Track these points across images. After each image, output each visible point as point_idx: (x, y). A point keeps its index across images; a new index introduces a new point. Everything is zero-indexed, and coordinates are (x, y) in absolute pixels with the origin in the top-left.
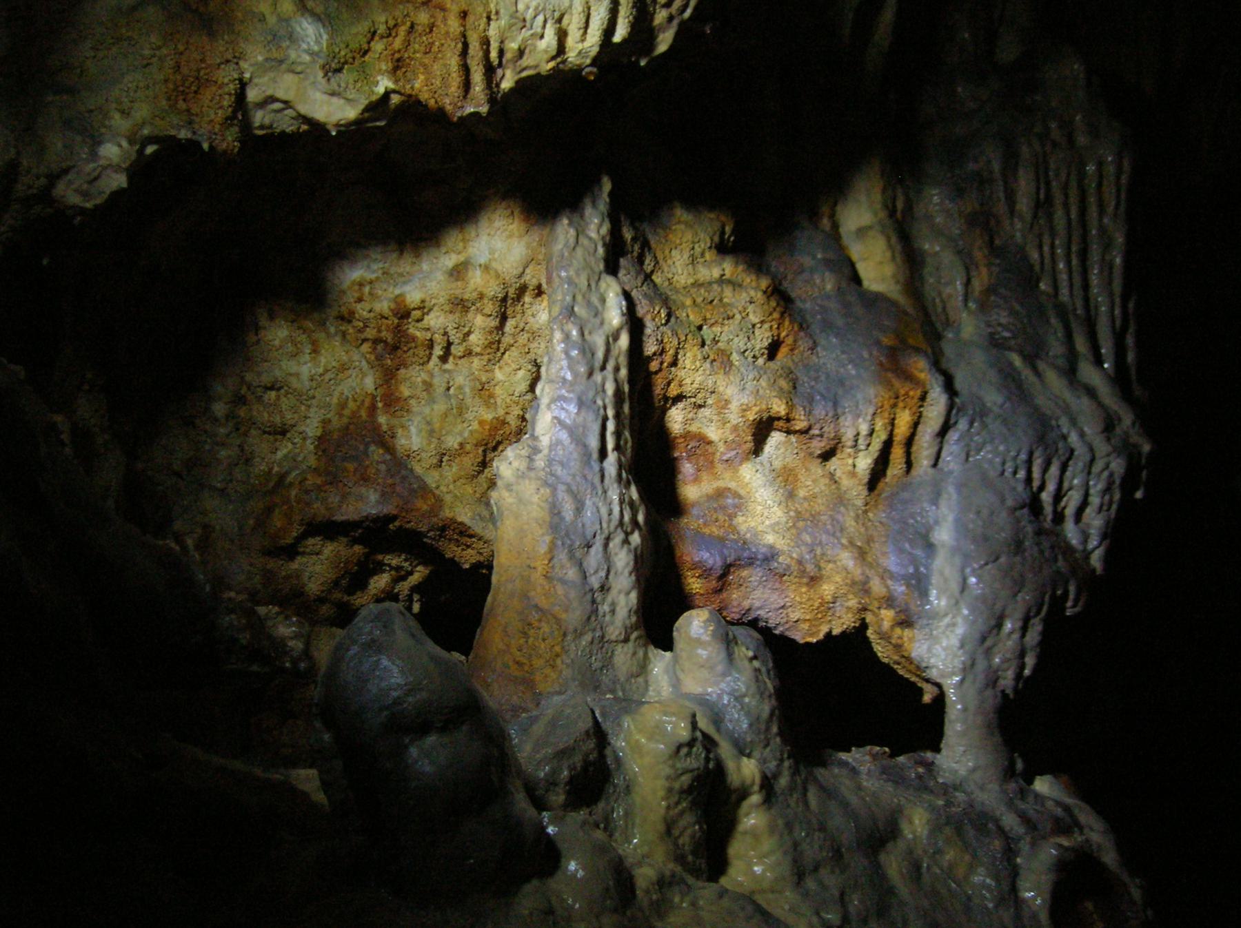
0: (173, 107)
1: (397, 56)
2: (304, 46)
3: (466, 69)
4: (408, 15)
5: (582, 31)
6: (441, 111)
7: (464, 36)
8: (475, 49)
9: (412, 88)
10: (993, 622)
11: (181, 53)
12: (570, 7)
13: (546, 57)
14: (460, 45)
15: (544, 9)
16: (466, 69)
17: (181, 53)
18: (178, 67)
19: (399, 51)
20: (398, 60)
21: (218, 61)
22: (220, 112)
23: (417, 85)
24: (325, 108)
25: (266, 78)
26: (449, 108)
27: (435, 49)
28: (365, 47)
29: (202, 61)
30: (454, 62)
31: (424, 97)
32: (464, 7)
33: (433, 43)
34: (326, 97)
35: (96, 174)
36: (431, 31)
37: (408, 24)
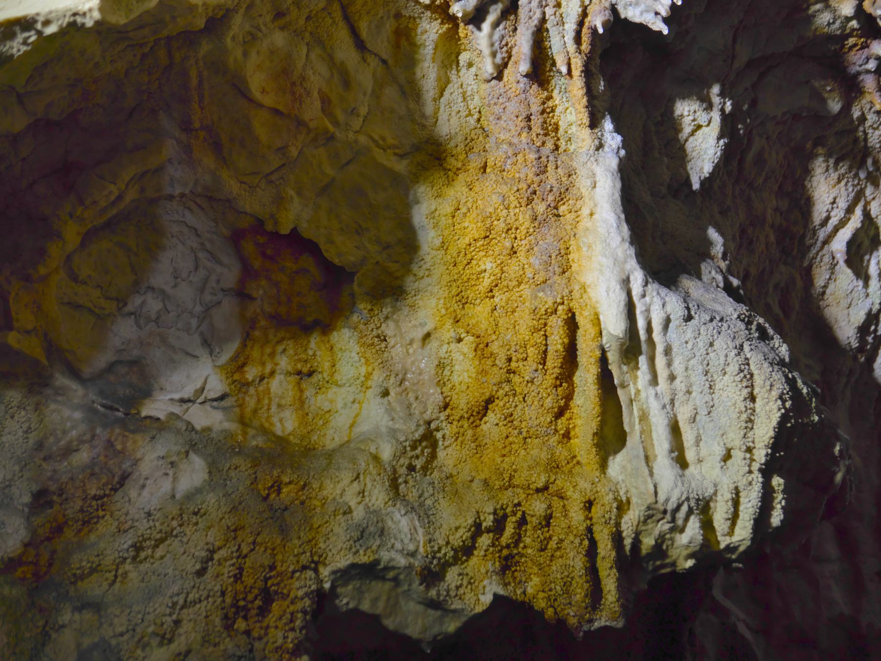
0: (228, 626)
1: (505, 552)
2: (398, 546)
3: (593, 571)
4: (519, 504)
5: (729, 522)
6: (561, 622)
7: (589, 530)
8: (605, 548)
9: (524, 593)
10: (245, 335)
11: (245, 556)
12: (715, 493)
13: (685, 553)
14: (586, 542)
15: (688, 499)
16: (593, 571)
17: (245, 556)
18: (238, 578)
19: (508, 546)
20: (506, 558)
21: (291, 568)
22: (291, 635)
23: (530, 591)
24: (420, 621)
25: (350, 587)
26: (573, 621)
27: (553, 544)
28: (469, 543)
29: (272, 567)
30: (579, 563)
31: (540, 604)
32: (590, 495)
33: (550, 538)
34: (420, 608)
35: (557, 340)
36: (548, 525)
37: (519, 514)
